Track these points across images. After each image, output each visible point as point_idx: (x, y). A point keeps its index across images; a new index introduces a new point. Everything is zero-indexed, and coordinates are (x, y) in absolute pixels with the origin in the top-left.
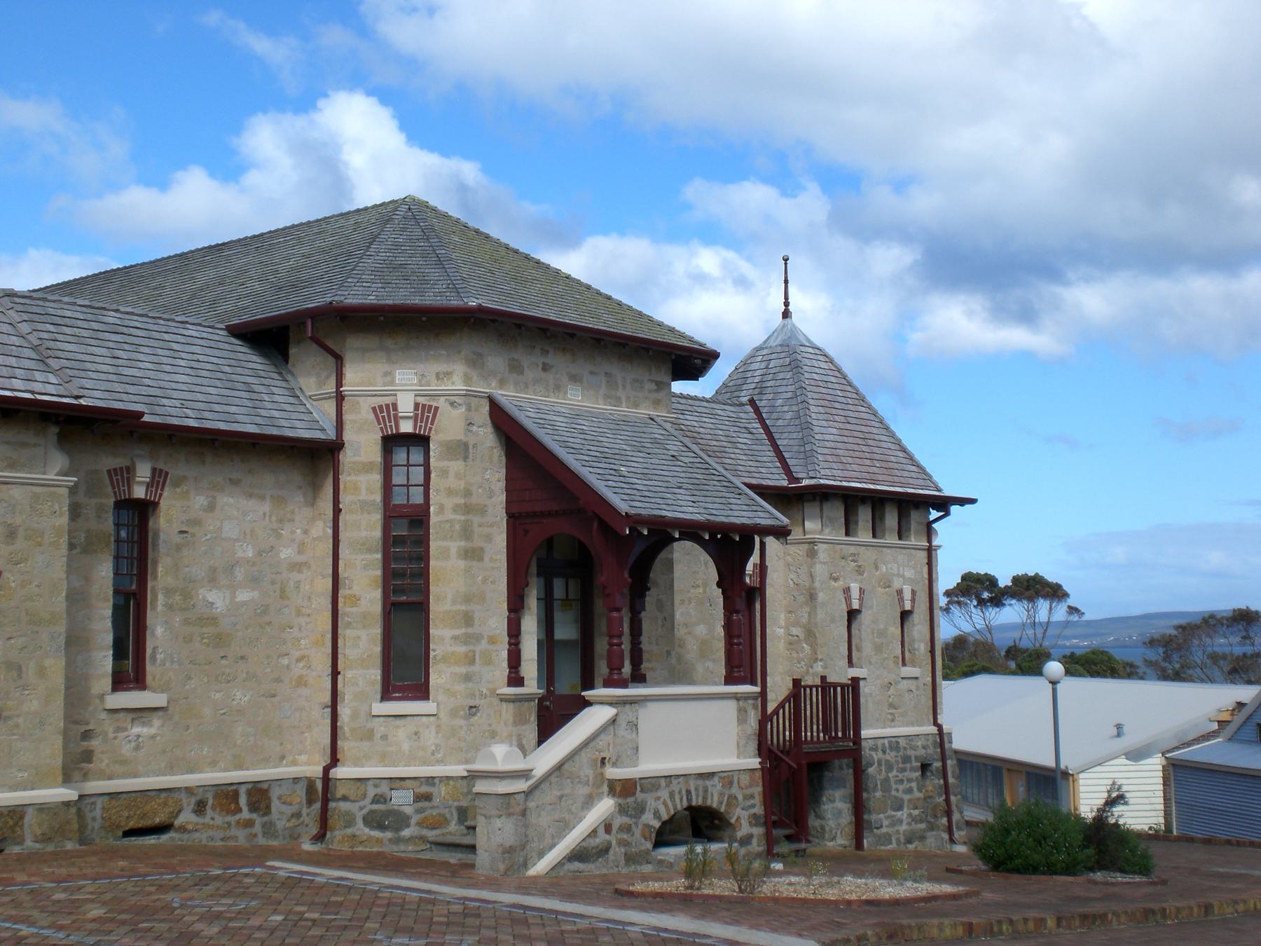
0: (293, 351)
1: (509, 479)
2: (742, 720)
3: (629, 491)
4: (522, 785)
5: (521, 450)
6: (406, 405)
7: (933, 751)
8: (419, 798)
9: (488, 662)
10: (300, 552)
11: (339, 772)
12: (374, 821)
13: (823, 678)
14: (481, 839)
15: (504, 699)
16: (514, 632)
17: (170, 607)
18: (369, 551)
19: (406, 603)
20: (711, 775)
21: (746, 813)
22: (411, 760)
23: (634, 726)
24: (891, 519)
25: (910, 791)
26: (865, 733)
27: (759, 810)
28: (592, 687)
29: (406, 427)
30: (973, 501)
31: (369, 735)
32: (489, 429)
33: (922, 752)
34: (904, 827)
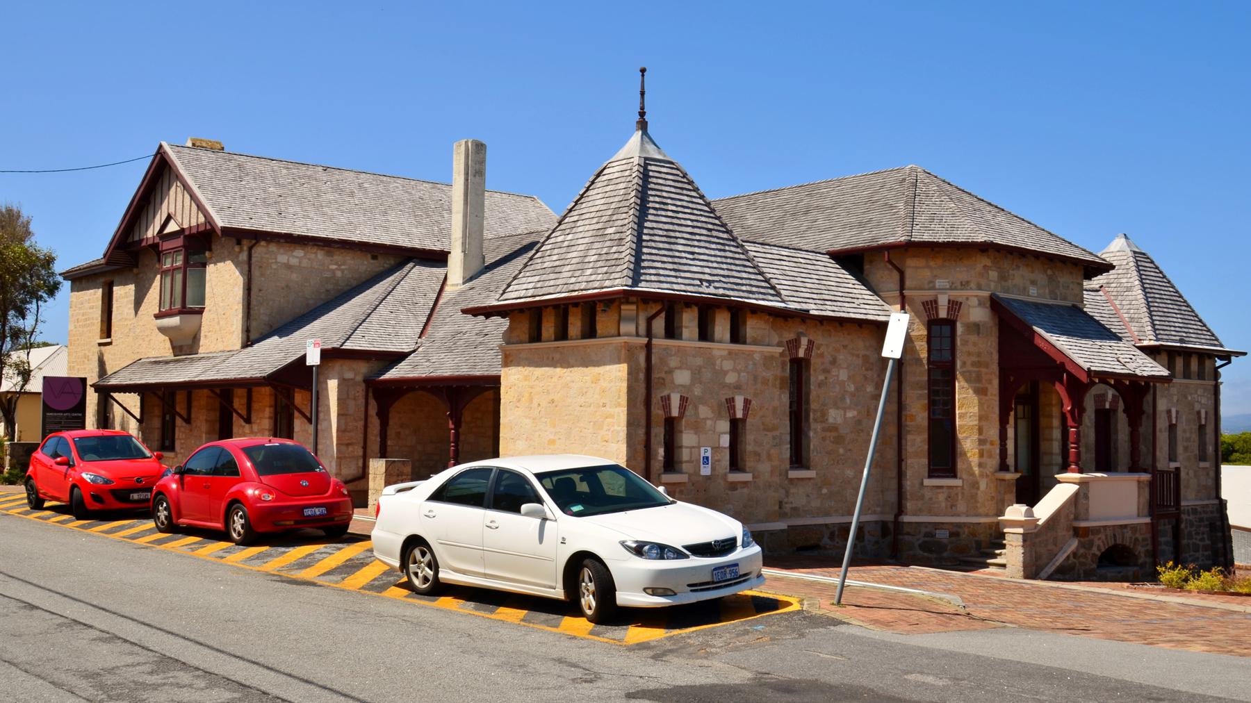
0: (867, 267)
8: (951, 535)
11: (906, 519)
20: (1125, 526)
28: (229, 435)
29: (943, 314)
30: (1245, 354)
33: (1210, 515)
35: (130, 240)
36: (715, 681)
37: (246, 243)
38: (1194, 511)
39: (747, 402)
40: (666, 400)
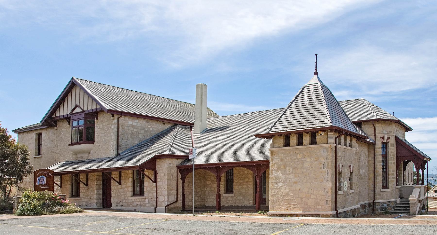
11: (376, 201)
31: (380, 195)
35: (54, 116)
37: (116, 116)
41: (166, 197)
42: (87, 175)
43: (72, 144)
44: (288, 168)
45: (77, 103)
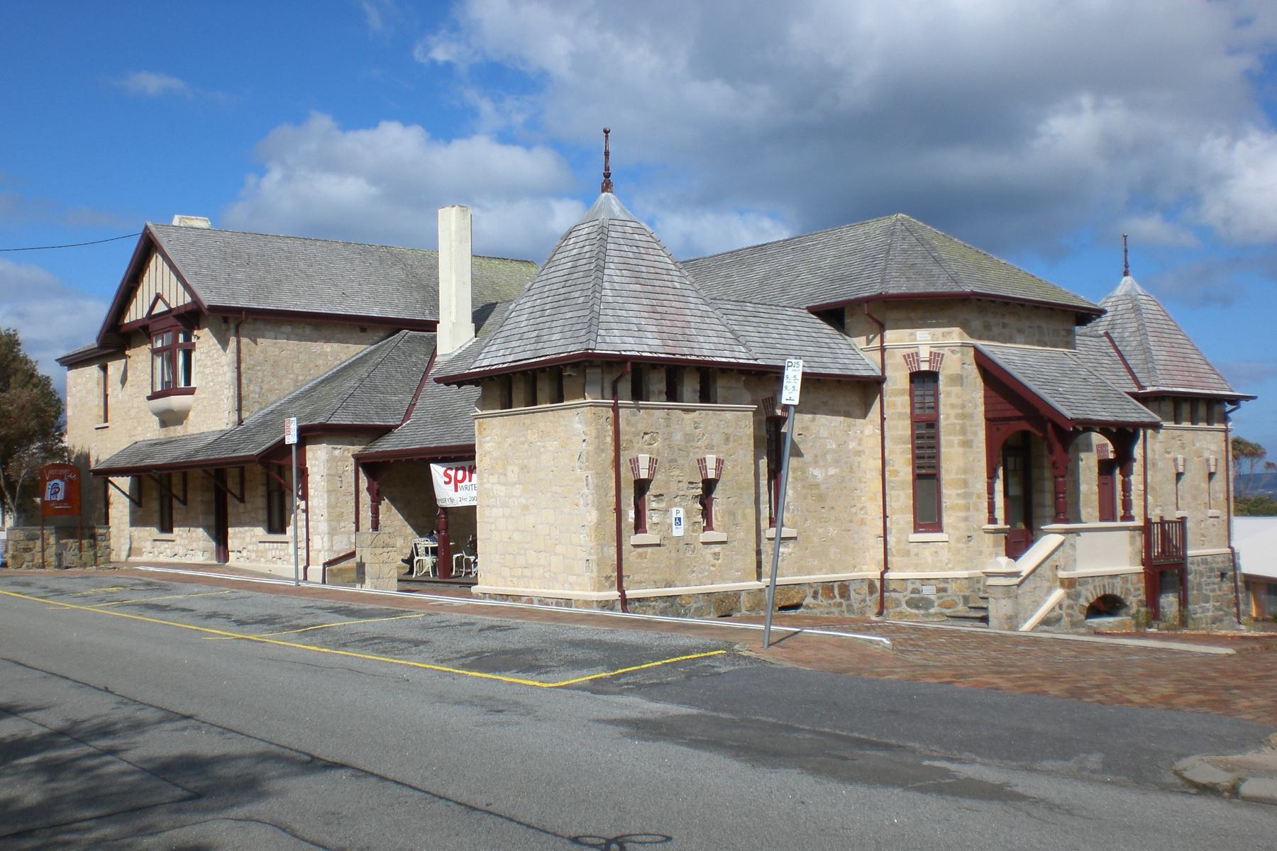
0: (848, 321)
1: (986, 397)
2: (1132, 542)
3: (1069, 402)
4: (1016, 581)
5: (995, 378)
6: (924, 353)
7: (1229, 565)
8: (939, 590)
9: (977, 510)
10: (860, 445)
11: (890, 575)
12: (913, 603)
13: (1162, 518)
14: (992, 614)
15: (987, 532)
16: (991, 491)
17: (795, 479)
18: (904, 443)
19: (927, 475)
21: (1135, 597)
22: (934, 568)
23: (1073, 546)
24: (1202, 410)
25: (1213, 590)
26: (1190, 553)
27: (1143, 597)
29: (925, 367)
31: (907, 554)
32: (975, 366)
33: (1221, 565)
34: (1210, 614)
36: (639, 715)
38: (1204, 560)
39: (720, 462)
40: (634, 461)
41: (326, 539)
42: (242, 471)
43: (154, 396)
44: (510, 468)
45: (160, 291)
